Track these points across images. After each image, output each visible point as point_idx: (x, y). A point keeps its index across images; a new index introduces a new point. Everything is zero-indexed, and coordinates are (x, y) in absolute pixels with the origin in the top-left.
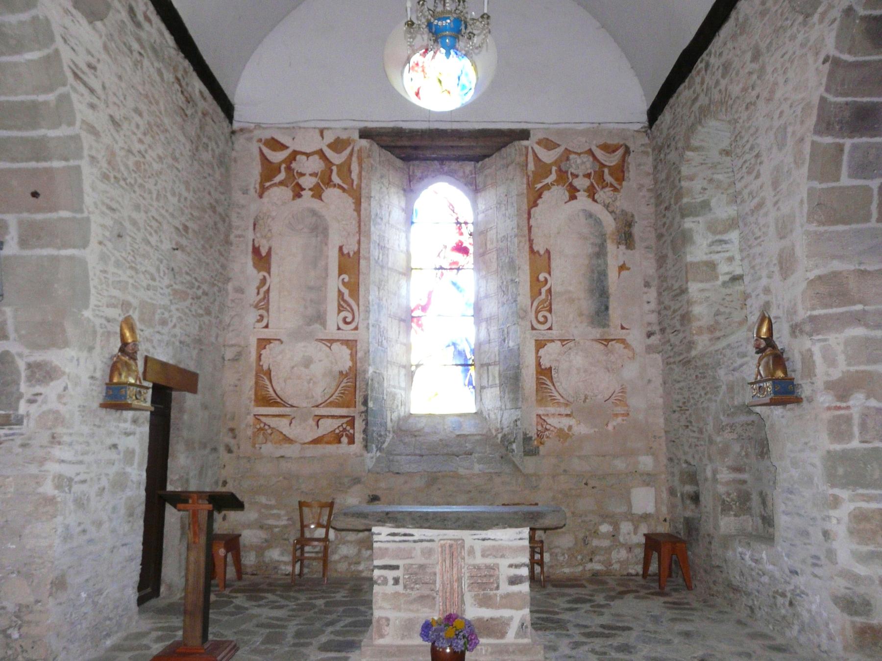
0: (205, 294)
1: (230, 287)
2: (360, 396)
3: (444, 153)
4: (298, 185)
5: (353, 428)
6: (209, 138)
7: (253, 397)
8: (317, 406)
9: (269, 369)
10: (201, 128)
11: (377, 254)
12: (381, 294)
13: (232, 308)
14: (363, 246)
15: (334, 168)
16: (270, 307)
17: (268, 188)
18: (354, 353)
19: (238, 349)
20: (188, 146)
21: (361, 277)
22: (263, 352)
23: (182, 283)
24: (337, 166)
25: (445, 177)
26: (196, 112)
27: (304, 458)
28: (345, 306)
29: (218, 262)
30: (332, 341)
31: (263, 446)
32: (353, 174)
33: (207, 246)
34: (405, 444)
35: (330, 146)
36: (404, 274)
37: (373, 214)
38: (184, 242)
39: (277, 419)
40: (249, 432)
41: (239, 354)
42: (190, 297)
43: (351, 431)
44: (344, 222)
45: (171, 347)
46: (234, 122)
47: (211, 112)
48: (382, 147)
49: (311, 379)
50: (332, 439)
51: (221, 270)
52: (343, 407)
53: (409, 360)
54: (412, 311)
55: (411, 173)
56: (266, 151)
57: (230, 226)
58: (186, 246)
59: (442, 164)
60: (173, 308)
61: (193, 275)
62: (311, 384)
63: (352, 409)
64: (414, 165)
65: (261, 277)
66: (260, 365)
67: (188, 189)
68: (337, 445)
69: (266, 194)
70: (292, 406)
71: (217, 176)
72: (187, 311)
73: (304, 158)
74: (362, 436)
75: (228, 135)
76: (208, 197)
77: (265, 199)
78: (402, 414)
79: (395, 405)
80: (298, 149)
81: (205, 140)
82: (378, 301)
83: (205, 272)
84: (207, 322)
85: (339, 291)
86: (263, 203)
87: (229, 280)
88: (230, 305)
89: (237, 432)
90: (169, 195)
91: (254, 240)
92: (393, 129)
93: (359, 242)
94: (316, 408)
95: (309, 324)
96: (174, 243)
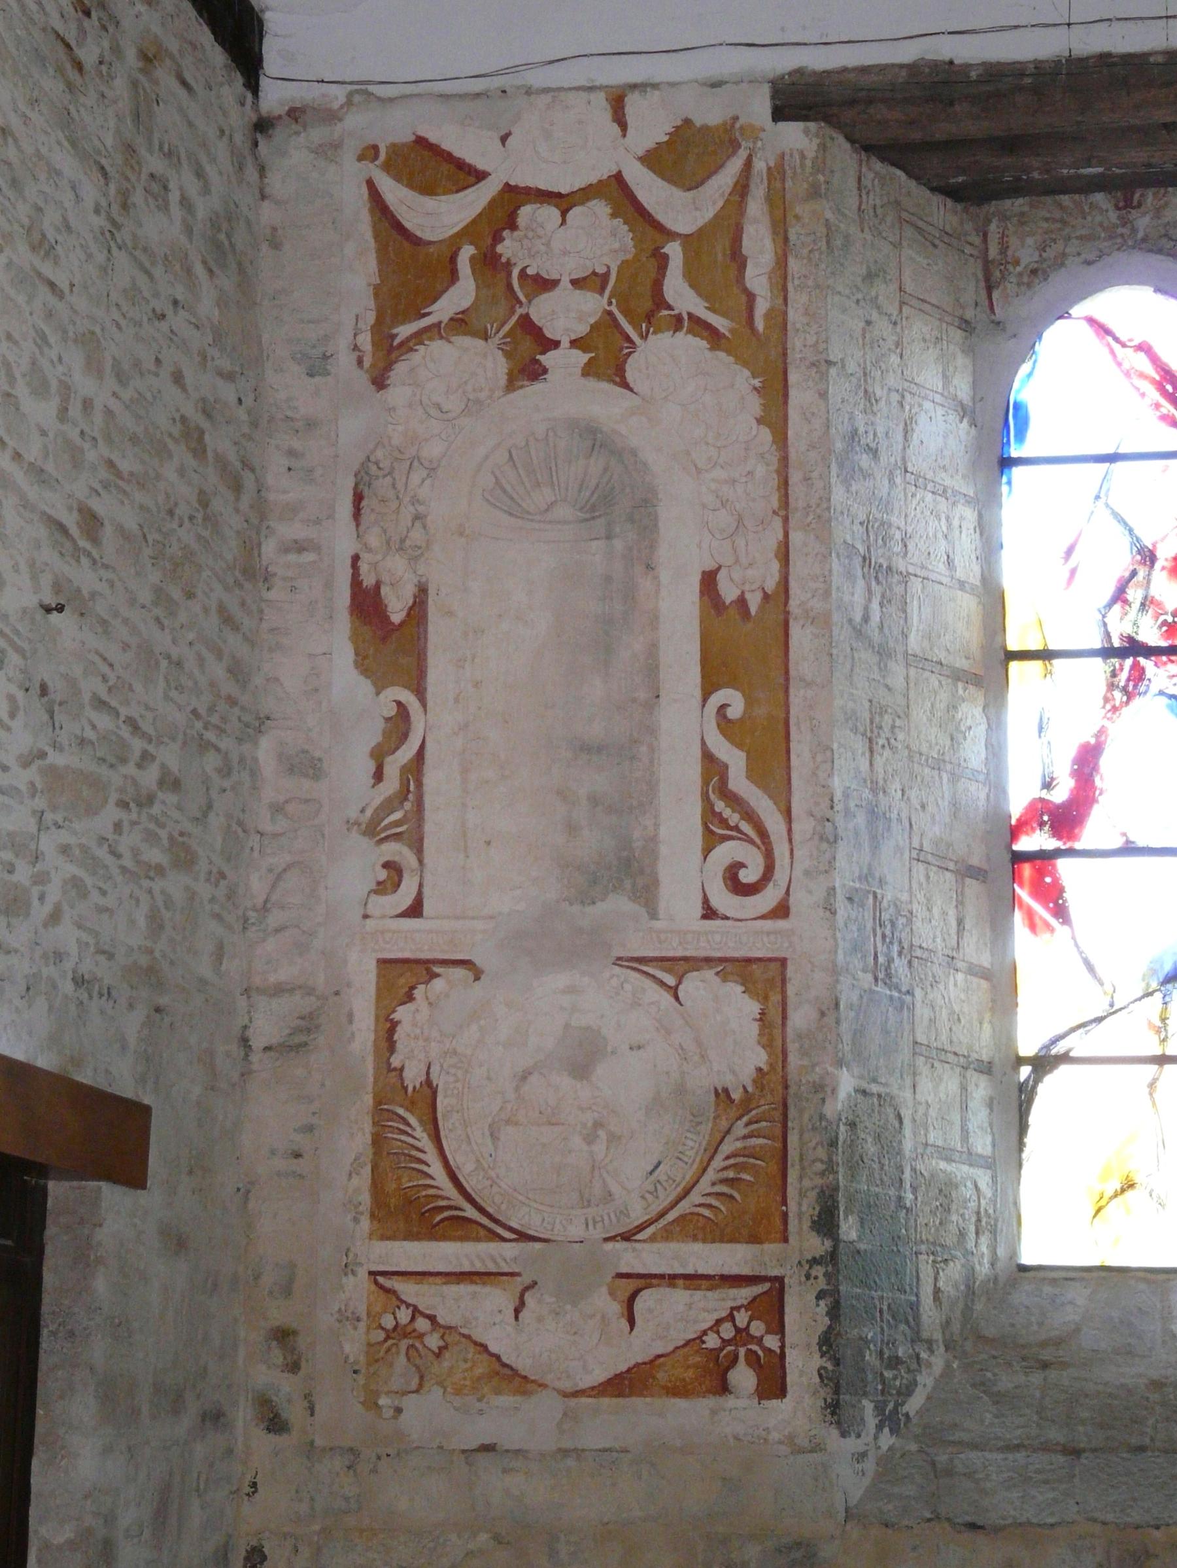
0: (170, 782)
1: (265, 751)
2: (802, 1194)
3: (1136, 156)
4: (526, 324)
5: (779, 1328)
6: (170, 154)
7: (366, 1198)
8: (627, 1237)
9: (428, 1082)
10: (137, 116)
11: (859, 598)
12: (879, 761)
13: (276, 835)
14: (798, 567)
15: (674, 250)
16: (428, 827)
17: (407, 346)
18: (774, 1014)
19: (299, 1003)
20: (90, 192)
21: (798, 697)
22: (402, 1013)
23: (82, 742)
24: (686, 239)
25: (1138, 259)
26: (116, 50)
27: (578, 1453)
28: (734, 818)
29: (219, 656)
30: (682, 965)
31: (410, 1403)
32: (750, 271)
33: (176, 593)
34: (998, 1398)
35: (652, 160)
36: (975, 680)
37: (840, 427)
38: (85, 578)
39: (463, 1289)
40: (354, 1345)
41: (308, 1024)
42: (114, 797)
43: (772, 1342)
44: (719, 473)
45: (41, 1003)
46: (264, 82)
47: (173, 45)
48: (868, 148)
49: (598, 1125)
50: (690, 1374)
51: (229, 687)
52: (732, 1240)
53: (1006, 1036)
54: (1015, 832)
55: (993, 252)
56: (394, 192)
57: (261, 508)
58: (93, 595)
59: (1128, 204)
60: (48, 843)
61: (124, 712)
62: (600, 1148)
63: (772, 1248)
64: (1004, 218)
65: (392, 711)
66: (390, 1069)
67: (93, 366)
68: (711, 1402)
69: (400, 369)
70: (523, 1237)
71: (207, 307)
72: (102, 853)
73: (549, 214)
74: (817, 1361)
75: (240, 139)
76: (171, 392)
77: (398, 393)
78: (983, 1269)
79: (953, 1228)
80: (524, 178)
81: (155, 163)
82: (866, 794)
83: (167, 697)
84: (178, 896)
85: (708, 757)
86: (391, 410)
87: (260, 724)
88: (268, 827)
89: (302, 1342)
90: (21, 390)
91: (356, 559)
92: (913, 68)
93: (784, 554)
94: (620, 1245)
95: (586, 898)
96: (46, 580)
